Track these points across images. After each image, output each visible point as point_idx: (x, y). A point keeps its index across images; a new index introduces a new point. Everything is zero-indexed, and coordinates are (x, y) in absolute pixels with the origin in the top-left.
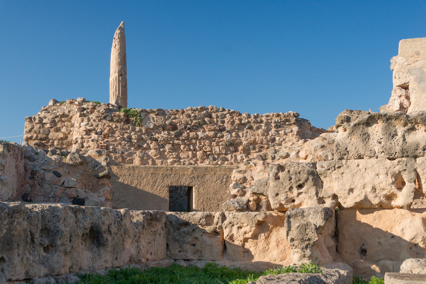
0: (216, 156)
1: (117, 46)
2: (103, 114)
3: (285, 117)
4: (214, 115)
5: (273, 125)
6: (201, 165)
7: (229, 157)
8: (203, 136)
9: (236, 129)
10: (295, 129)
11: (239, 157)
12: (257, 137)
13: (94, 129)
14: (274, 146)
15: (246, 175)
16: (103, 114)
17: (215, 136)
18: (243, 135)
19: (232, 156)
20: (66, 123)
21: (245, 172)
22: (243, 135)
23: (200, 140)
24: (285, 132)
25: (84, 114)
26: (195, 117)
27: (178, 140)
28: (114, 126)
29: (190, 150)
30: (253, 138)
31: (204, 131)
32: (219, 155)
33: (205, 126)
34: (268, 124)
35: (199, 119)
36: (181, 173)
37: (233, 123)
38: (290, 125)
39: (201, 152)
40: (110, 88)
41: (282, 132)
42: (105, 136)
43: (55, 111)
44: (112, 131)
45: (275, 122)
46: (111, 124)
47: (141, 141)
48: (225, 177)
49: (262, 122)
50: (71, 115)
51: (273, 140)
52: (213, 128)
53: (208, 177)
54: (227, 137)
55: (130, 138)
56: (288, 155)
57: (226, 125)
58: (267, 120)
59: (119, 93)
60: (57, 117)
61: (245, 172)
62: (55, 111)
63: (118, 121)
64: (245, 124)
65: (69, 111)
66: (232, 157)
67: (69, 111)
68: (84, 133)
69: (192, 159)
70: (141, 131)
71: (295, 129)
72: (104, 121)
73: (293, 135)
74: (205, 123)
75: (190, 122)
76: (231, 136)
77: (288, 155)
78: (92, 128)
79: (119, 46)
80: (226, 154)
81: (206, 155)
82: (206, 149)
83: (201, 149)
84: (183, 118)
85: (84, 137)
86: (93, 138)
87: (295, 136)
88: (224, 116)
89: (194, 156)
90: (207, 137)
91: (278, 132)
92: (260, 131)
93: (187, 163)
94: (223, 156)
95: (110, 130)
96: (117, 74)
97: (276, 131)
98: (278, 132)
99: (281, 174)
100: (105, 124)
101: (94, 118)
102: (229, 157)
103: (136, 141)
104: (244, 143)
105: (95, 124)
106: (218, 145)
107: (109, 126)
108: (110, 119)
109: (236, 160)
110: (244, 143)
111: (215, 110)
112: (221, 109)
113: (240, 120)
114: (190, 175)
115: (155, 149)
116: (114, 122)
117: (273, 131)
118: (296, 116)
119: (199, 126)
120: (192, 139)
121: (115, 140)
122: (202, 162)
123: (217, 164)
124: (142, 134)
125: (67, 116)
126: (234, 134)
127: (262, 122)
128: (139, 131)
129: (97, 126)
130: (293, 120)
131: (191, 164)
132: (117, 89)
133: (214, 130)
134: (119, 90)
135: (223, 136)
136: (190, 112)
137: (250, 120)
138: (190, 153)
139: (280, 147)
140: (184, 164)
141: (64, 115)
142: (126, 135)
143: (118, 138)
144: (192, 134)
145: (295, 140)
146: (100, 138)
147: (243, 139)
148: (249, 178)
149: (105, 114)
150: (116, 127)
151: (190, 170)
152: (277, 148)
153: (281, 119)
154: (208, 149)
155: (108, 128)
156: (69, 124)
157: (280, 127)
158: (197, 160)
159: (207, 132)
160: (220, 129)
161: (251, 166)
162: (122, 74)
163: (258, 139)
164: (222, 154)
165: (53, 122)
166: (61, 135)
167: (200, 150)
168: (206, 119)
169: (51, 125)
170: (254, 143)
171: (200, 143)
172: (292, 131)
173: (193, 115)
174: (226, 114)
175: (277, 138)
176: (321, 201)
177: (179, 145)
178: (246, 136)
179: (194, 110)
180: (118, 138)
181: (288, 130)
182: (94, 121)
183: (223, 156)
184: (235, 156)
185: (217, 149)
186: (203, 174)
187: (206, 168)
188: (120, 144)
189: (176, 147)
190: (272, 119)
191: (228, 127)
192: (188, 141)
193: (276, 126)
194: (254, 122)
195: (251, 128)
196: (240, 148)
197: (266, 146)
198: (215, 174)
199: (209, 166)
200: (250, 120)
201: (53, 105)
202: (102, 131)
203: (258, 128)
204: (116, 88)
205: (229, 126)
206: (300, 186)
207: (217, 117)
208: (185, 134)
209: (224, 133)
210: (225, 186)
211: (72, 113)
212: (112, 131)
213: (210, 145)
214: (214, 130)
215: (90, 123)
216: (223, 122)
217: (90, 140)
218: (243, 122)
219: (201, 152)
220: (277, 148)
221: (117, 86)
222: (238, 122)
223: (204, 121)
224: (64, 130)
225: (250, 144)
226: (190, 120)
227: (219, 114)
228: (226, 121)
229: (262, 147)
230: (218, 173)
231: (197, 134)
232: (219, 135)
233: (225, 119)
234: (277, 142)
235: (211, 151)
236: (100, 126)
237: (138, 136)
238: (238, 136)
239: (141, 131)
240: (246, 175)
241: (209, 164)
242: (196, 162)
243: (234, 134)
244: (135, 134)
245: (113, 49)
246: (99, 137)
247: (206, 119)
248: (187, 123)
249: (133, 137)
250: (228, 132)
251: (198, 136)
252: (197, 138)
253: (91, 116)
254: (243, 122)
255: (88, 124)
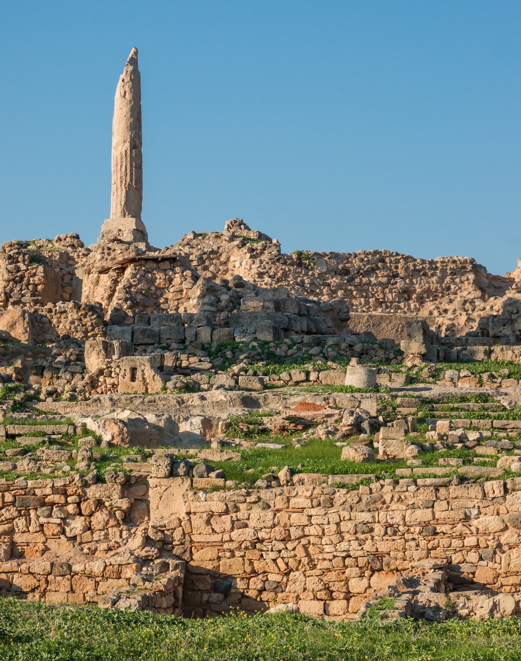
0: (389, 304)
1: (127, 94)
2: (276, 256)
3: (461, 263)
4: (387, 260)
5: (449, 272)
6: (374, 313)
7: (402, 305)
8: (375, 282)
9: (409, 275)
10: (471, 276)
11: (412, 306)
12: (432, 285)
13: (267, 272)
14: (449, 294)
15: (454, 322)
16: (276, 256)
17: (389, 282)
18: (417, 282)
19: (405, 304)
20: (214, 261)
21: (453, 319)
22: (417, 282)
23: (372, 286)
24: (460, 280)
25: (254, 255)
26: (368, 261)
27: (350, 285)
28: (287, 269)
29: (362, 296)
30: (427, 285)
31: (377, 277)
32: (392, 303)
33: (378, 272)
34: (444, 271)
35: (372, 264)
36: (357, 321)
37: (407, 269)
38: (466, 272)
39: (374, 299)
40: (112, 170)
41: (457, 280)
42: (278, 281)
43: (199, 247)
44: (285, 275)
45: (451, 269)
46: (284, 267)
47: (313, 286)
48: (400, 326)
49: (437, 268)
50: (220, 251)
51: (449, 288)
52: (386, 273)
53: (383, 325)
54: (400, 284)
55: (303, 282)
56: (484, 309)
57: (399, 271)
58: (443, 266)
59: (131, 180)
60: (205, 253)
61: (453, 319)
62: (199, 247)
63: (292, 264)
64: (419, 271)
65: (219, 248)
66: (405, 306)
67: (219, 248)
68: (257, 276)
69: (364, 306)
70: (313, 275)
71: (471, 276)
72: (278, 264)
73: (469, 284)
74: (378, 268)
75: (363, 267)
76: (405, 283)
77: (484, 309)
78: (265, 270)
79: (131, 95)
80: (399, 302)
81: (379, 303)
82: (378, 295)
83: (373, 295)
84: (356, 263)
85: (257, 280)
86: (266, 281)
87: (471, 285)
88: (397, 261)
89: (367, 303)
90: (380, 284)
91: (453, 280)
92: (434, 279)
93: (359, 310)
94: (396, 304)
95: (283, 273)
96: (128, 145)
97: (451, 278)
98: (453, 280)
99: (495, 320)
100: (278, 267)
101: (266, 260)
102: (402, 305)
103: (308, 286)
104: (418, 290)
105: (267, 267)
106: (391, 292)
107: (282, 269)
108: (283, 261)
109: (409, 309)
110: (418, 290)
111: (388, 255)
112: (394, 254)
113: (415, 266)
114: (366, 323)
115: (327, 294)
116: (287, 265)
117: (448, 279)
118: (472, 261)
119: (373, 270)
120: (364, 285)
121: (289, 285)
122: (375, 310)
123: (389, 312)
124: (315, 278)
125: (217, 252)
126: (407, 281)
127: (437, 268)
128: (311, 276)
129: (270, 268)
130: (469, 267)
131: (364, 312)
132: (128, 172)
133: (387, 276)
134: (131, 174)
135: (396, 283)
136: (363, 256)
137: (424, 266)
138: (362, 300)
139: (455, 296)
140: (357, 311)
141: (213, 252)
142: (299, 280)
143: (291, 282)
144: (365, 280)
145: (471, 289)
146: (273, 282)
147: (417, 286)
148: (457, 324)
149: (278, 257)
150: (290, 270)
151: (366, 318)
152: (452, 297)
153: (456, 266)
154: (381, 296)
155: (281, 272)
156: (218, 262)
157: (455, 274)
158: (370, 307)
159: (380, 279)
160: (393, 275)
161: (457, 316)
162: (135, 145)
163: (433, 287)
164: (395, 302)
165: (201, 260)
166: (209, 275)
167: (372, 297)
168: (380, 265)
169: (198, 262)
170: (428, 291)
171: (373, 290)
172: (468, 279)
173: (366, 259)
174: (400, 259)
175: (452, 287)
176: (514, 332)
177: (351, 291)
178: (420, 283)
179: (367, 254)
180: (291, 282)
181: (464, 278)
182: (267, 263)
183: (396, 304)
184: (409, 305)
185: (390, 296)
186: (378, 322)
187: (382, 317)
188: (293, 288)
189: (348, 292)
190: (447, 265)
191: (401, 272)
192: (362, 289)
193: (452, 273)
194: (429, 268)
195: (425, 274)
196: (414, 296)
197: (440, 295)
198: (390, 323)
199: (382, 314)
200: (424, 266)
201: (194, 239)
202: (275, 274)
203: (433, 275)
204: (126, 170)
205: (403, 272)
206: (504, 326)
207: (391, 262)
208: (357, 280)
209: (398, 280)
210: (400, 336)
211: (221, 249)
212: (285, 275)
213: (383, 292)
214: (387, 276)
215: (262, 265)
216: (397, 267)
217: (263, 283)
218: (417, 268)
219: (374, 299)
220: (452, 297)
221: (128, 166)
222: (412, 268)
223: (377, 266)
224: (212, 268)
225: (424, 291)
226: (363, 265)
227: (393, 259)
228: (400, 267)
229: (436, 296)
230: (394, 322)
231: (369, 280)
232: (392, 281)
233: (399, 265)
234: (452, 291)
235: (384, 298)
236: (273, 269)
237: (312, 280)
238: (412, 283)
239: (313, 275)
240: (454, 322)
241: (382, 311)
242: (368, 309)
243: (407, 281)
244: (308, 278)
245: (118, 95)
246: (272, 281)
247: (380, 265)
248: (360, 268)
249: (306, 282)
250: (402, 278)
251: (370, 282)
252: (369, 283)
253: (262, 258)
254: (417, 268)
255: (261, 266)
